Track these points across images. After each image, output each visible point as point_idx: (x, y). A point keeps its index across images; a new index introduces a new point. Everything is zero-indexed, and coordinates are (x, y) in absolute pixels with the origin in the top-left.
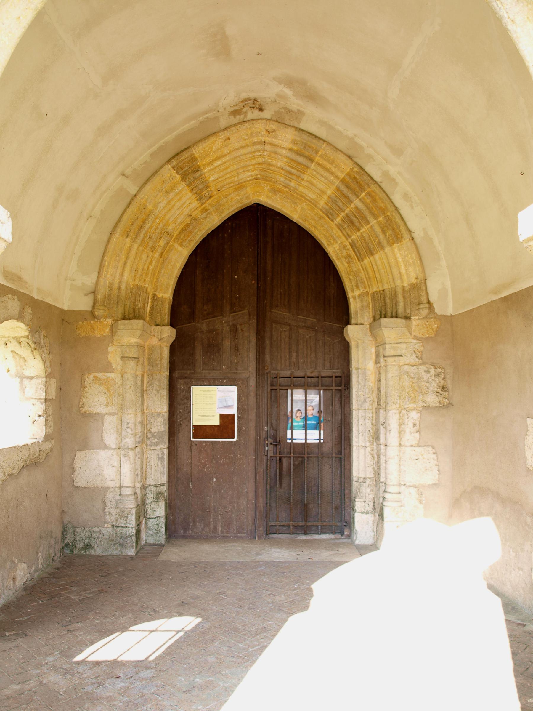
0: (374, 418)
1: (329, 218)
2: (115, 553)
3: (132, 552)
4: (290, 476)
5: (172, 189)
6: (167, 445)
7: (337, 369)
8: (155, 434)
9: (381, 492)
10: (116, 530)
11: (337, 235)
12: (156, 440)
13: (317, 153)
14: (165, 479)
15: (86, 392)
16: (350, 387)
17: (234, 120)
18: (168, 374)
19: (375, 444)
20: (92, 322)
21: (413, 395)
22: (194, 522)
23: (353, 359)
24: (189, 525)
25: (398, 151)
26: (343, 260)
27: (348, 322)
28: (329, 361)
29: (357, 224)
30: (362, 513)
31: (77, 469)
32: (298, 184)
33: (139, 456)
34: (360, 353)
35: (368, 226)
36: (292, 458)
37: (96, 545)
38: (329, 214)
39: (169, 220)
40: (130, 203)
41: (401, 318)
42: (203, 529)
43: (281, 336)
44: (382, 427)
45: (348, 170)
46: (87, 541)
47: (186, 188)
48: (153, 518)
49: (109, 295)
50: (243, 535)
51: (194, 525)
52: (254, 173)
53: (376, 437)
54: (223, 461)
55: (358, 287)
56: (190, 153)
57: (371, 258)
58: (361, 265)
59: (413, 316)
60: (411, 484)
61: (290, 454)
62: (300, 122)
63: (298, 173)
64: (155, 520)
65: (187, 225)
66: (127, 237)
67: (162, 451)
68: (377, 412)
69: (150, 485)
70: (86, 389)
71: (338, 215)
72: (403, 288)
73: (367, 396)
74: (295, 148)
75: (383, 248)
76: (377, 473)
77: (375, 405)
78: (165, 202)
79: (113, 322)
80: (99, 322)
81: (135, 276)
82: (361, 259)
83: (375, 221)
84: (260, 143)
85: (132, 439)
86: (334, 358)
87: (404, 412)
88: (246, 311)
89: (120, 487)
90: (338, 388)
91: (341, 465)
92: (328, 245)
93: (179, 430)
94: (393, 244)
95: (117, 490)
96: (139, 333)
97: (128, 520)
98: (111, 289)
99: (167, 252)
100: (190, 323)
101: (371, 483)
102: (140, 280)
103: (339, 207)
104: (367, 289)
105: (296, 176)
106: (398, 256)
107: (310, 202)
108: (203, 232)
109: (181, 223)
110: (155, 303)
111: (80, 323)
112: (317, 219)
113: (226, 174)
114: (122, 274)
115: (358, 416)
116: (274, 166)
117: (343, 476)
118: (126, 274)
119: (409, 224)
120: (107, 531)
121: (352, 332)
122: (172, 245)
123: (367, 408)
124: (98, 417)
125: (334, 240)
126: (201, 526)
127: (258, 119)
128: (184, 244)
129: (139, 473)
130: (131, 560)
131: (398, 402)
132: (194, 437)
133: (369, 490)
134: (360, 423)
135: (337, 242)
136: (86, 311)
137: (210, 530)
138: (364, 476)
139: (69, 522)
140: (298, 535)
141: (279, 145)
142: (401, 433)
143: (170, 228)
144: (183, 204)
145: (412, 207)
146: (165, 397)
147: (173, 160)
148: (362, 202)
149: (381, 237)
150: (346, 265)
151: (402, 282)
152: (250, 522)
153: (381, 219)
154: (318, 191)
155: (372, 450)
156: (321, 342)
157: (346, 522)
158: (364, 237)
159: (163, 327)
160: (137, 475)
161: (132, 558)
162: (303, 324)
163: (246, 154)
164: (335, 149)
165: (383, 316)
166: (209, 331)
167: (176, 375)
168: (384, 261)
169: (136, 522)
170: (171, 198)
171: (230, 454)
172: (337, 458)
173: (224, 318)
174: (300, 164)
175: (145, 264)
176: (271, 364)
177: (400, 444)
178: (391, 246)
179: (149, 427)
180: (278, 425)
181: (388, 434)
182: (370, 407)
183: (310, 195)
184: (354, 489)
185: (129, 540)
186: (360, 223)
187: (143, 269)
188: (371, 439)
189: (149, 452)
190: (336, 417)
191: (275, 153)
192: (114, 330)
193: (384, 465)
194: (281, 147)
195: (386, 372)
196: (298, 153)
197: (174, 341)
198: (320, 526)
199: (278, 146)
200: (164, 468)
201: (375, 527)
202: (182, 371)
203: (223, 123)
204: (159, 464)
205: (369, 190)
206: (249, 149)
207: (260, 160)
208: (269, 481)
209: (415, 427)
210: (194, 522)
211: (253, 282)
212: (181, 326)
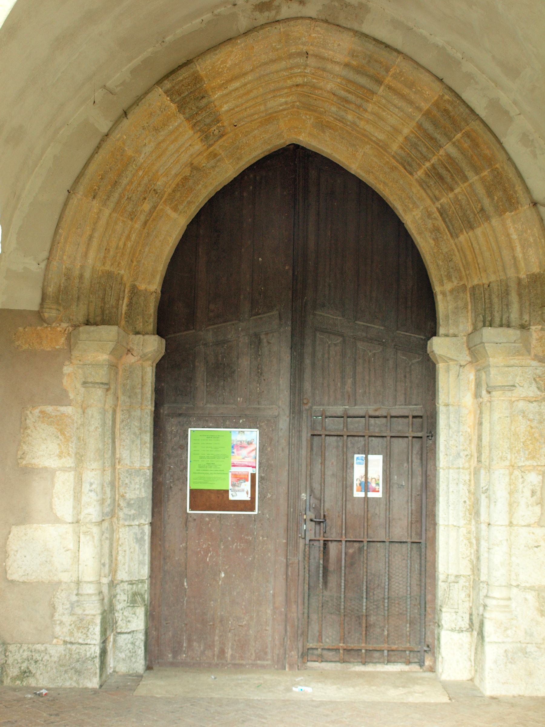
0: (472, 482)
1: (405, 169)
2: (68, 684)
3: (94, 683)
4: (341, 572)
5: (164, 125)
6: (149, 519)
7: (416, 405)
8: (132, 502)
9: (482, 597)
10: (70, 650)
11: (418, 196)
12: (133, 512)
13: (387, 70)
14: (145, 572)
15: (28, 435)
16: (435, 432)
17: (262, 18)
18: (153, 409)
19: (473, 522)
20: (39, 328)
21: (531, 447)
22: (190, 641)
23: (440, 389)
24: (182, 646)
25: (513, 72)
26: (428, 234)
27: (434, 333)
28: (403, 392)
29: (449, 180)
30: (452, 630)
32: (358, 117)
33: (108, 535)
34: (452, 379)
35: (466, 184)
36: (344, 542)
37: (39, 672)
38: (405, 164)
39: (157, 172)
40: (98, 147)
41: (514, 327)
42: (203, 653)
43: (329, 353)
44: (483, 496)
45: (436, 98)
47: (185, 123)
48: (126, 633)
49: (66, 287)
50: (265, 663)
51: (190, 646)
52: (289, 99)
53: (474, 511)
54: (236, 546)
55: (449, 278)
56: (192, 71)
57: (471, 233)
58: (456, 244)
59: (534, 325)
60: (528, 585)
61: (342, 537)
62: (362, 22)
63: (359, 101)
64: (129, 636)
65: (186, 179)
66: (94, 198)
67: (142, 529)
68: (476, 472)
69: (122, 581)
70: (29, 431)
71: (420, 167)
72: (519, 281)
73: (461, 447)
74: (354, 63)
75: (488, 219)
76: (476, 569)
77: (474, 462)
78: (153, 145)
79: (71, 329)
80: (49, 329)
81: (105, 258)
82: (454, 235)
83: (476, 178)
84: (299, 54)
85: (98, 508)
86: (411, 387)
87: (517, 472)
88: (275, 313)
89: (78, 583)
90: (417, 435)
91: (420, 555)
92: (404, 210)
93: (168, 496)
94: (505, 212)
95: (73, 585)
96: (111, 346)
97: (89, 634)
98: (68, 277)
99: (154, 220)
101: (467, 584)
102: (112, 264)
103: (421, 153)
104: (464, 281)
105: (356, 105)
106: (512, 231)
107: (377, 144)
108: (210, 189)
109: (176, 175)
110: (134, 299)
111: (21, 329)
112: (388, 170)
113: (247, 102)
114: (85, 255)
115: (448, 478)
116: (321, 89)
117: (423, 573)
118: (92, 254)
119: (530, 183)
120: (56, 651)
121: (438, 346)
122: (162, 210)
123: (461, 466)
124: (51, 473)
125: (414, 203)
126: (200, 647)
127: (297, 18)
128: (181, 207)
129: (107, 561)
130: (94, 694)
131: (509, 457)
132: (192, 508)
133: (463, 595)
134: (451, 490)
135: (418, 207)
136: (30, 311)
137: (214, 655)
138: (456, 573)
140: (350, 665)
141: (330, 57)
142: (512, 505)
143: (159, 183)
144: (180, 147)
145: (535, 156)
146: (148, 445)
147: (166, 82)
148: (457, 147)
149: (486, 202)
150: (432, 242)
151: (517, 270)
152: (277, 642)
153: (485, 173)
154: (389, 129)
155: (469, 533)
156: (391, 363)
157: (428, 646)
158: (459, 201)
159: (147, 337)
160: (104, 565)
161: (95, 692)
162: (364, 334)
163: (277, 72)
164: (416, 66)
165: (487, 323)
166: (218, 344)
167: (165, 410)
168: (490, 238)
169: (101, 639)
170: (161, 138)
171: (247, 535)
172: (415, 545)
174: (362, 87)
175: (120, 239)
176: (313, 394)
177: (511, 522)
178: (501, 215)
179: (122, 490)
180: (322, 490)
181: (492, 506)
182: (467, 465)
183: (376, 134)
184: (440, 593)
185: (89, 664)
186: (453, 179)
187: (117, 248)
188: (468, 515)
189: (122, 530)
190: (414, 480)
191: (324, 70)
192: (72, 340)
193: (486, 555)
194: (332, 61)
195: (491, 410)
196: (358, 70)
197: (163, 358)
198: (386, 652)
199: (328, 59)
200: (144, 555)
201: (473, 654)
202: (175, 405)
203: (244, 23)
204: (137, 548)
205: (467, 128)
206: (283, 64)
207: (299, 80)
208: (307, 578)
209: (535, 497)
210: (190, 641)
211: (287, 268)
212: (173, 335)
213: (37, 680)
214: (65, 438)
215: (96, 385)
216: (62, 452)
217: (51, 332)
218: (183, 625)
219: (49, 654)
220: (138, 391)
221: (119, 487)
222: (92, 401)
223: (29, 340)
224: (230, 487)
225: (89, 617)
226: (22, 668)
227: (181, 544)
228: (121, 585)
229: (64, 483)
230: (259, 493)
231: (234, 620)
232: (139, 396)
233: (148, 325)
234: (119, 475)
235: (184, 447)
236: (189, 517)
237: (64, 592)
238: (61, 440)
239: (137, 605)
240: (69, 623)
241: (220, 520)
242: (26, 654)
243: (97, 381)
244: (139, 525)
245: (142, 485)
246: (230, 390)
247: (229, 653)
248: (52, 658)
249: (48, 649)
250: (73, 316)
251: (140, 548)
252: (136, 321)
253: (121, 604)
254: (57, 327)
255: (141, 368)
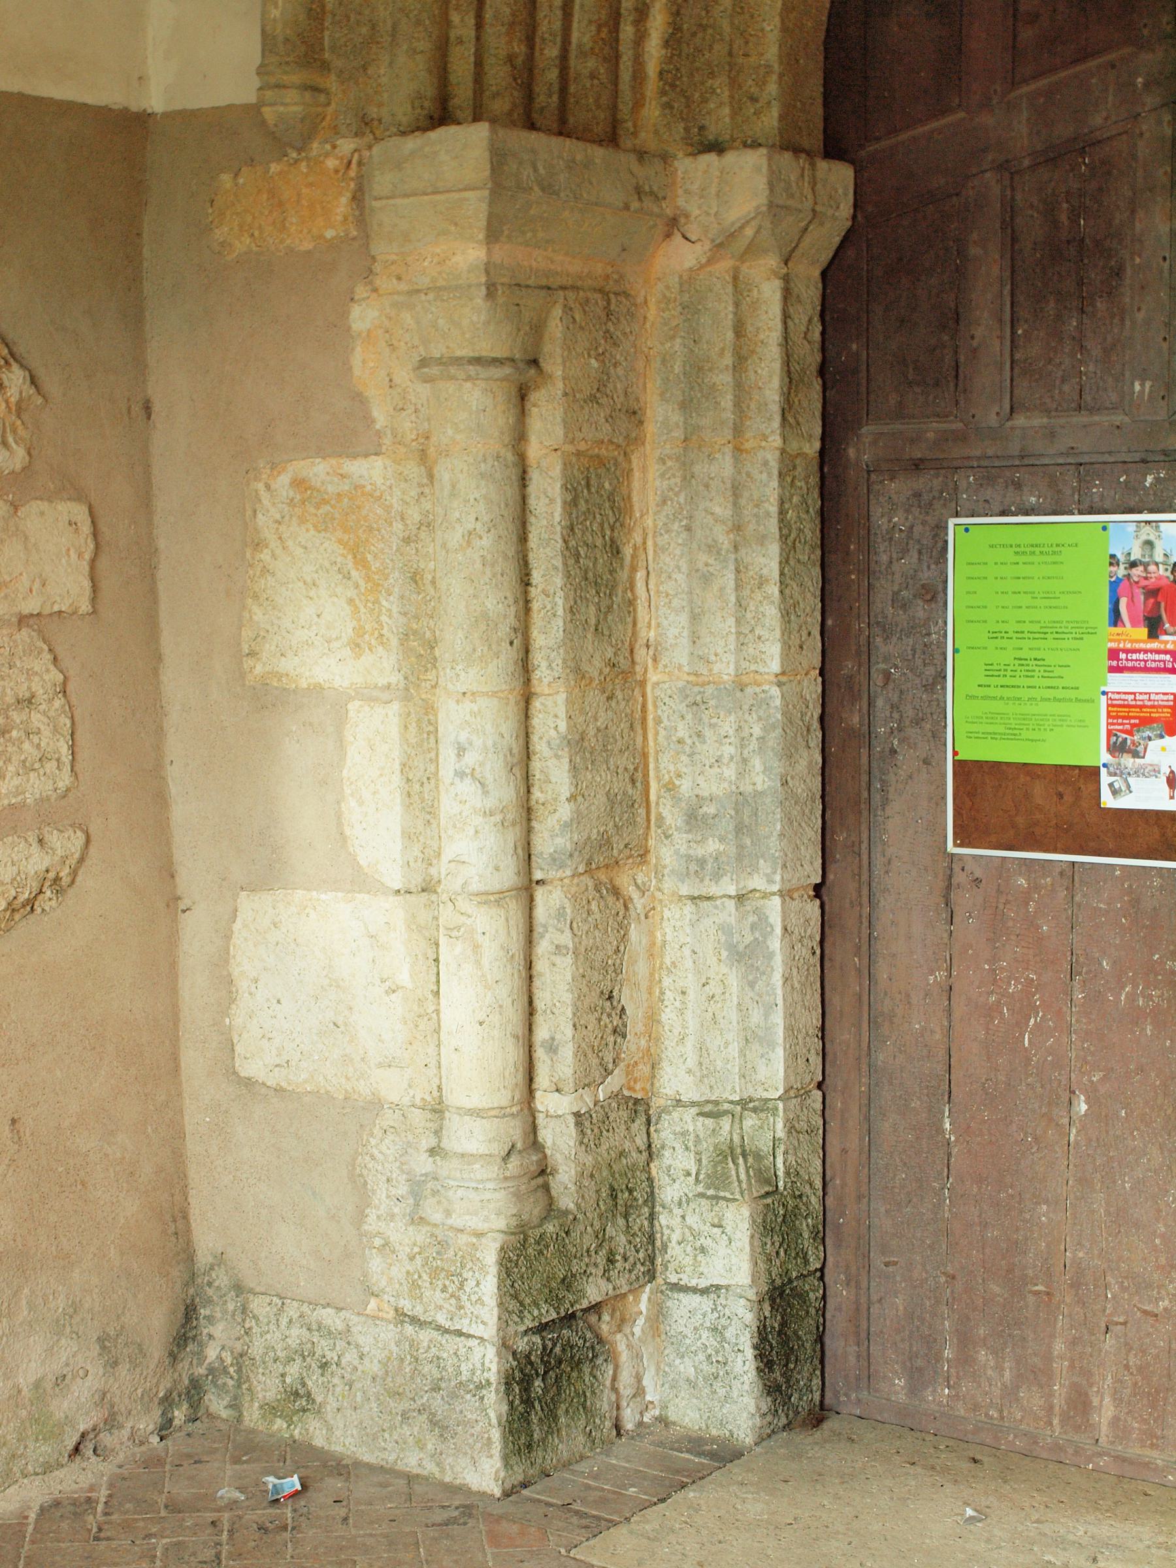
8: (710, 810)
12: (713, 845)
14: (772, 1073)
15: (265, 571)
20: (274, 168)
22: (965, 1341)
24: (938, 1358)
31: (243, 985)
42: (1010, 1393)
46: (294, 1370)
48: (694, 1290)
51: (965, 1359)
54: (1132, 998)
64: (705, 1303)
70: (265, 556)
80: (303, 167)
95: (418, 1118)
96: (476, 206)
100: (944, 112)
111: (226, 179)
120: (376, 1340)
126: (1000, 1369)
132: (964, 836)
139: (220, 1259)
166: (1051, 157)
167: (862, 449)
173: (1146, 57)
200: (769, 1009)
202: (898, 426)
210: (965, 1341)
213: (330, 1429)
214: (368, 579)
215: (453, 370)
216: (360, 631)
217: (311, 179)
218: (943, 1279)
219: (357, 1346)
220: (724, 379)
221: (657, 752)
222: (450, 432)
223: (249, 219)
224: (1105, 757)
225: (463, 1239)
226: (288, 1380)
227: (932, 972)
228: (675, 1115)
229: (372, 741)
230: (946, 812)
231: (1124, 1289)
232: (727, 401)
233: (757, 113)
234: (656, 706)
235: (934, 594)
236: (957, 868)
237: (390, 1137)
238: (357, 587)
239: (728, 1195)
240: (408, 1250)
241: (1071, 889)
242: (296, 1334)
243: (459, 353)
244: (740, 898)
245: (754, 745)
246: (1107, 351)
247: (1105, 1411)
248: (366, 1361)
249: (354, 1330)
250: (380, 105)
251: (752, 985)
252: (705, 101)
253: (676, 1186)
254: (327, 155)
255: (730, 289)
